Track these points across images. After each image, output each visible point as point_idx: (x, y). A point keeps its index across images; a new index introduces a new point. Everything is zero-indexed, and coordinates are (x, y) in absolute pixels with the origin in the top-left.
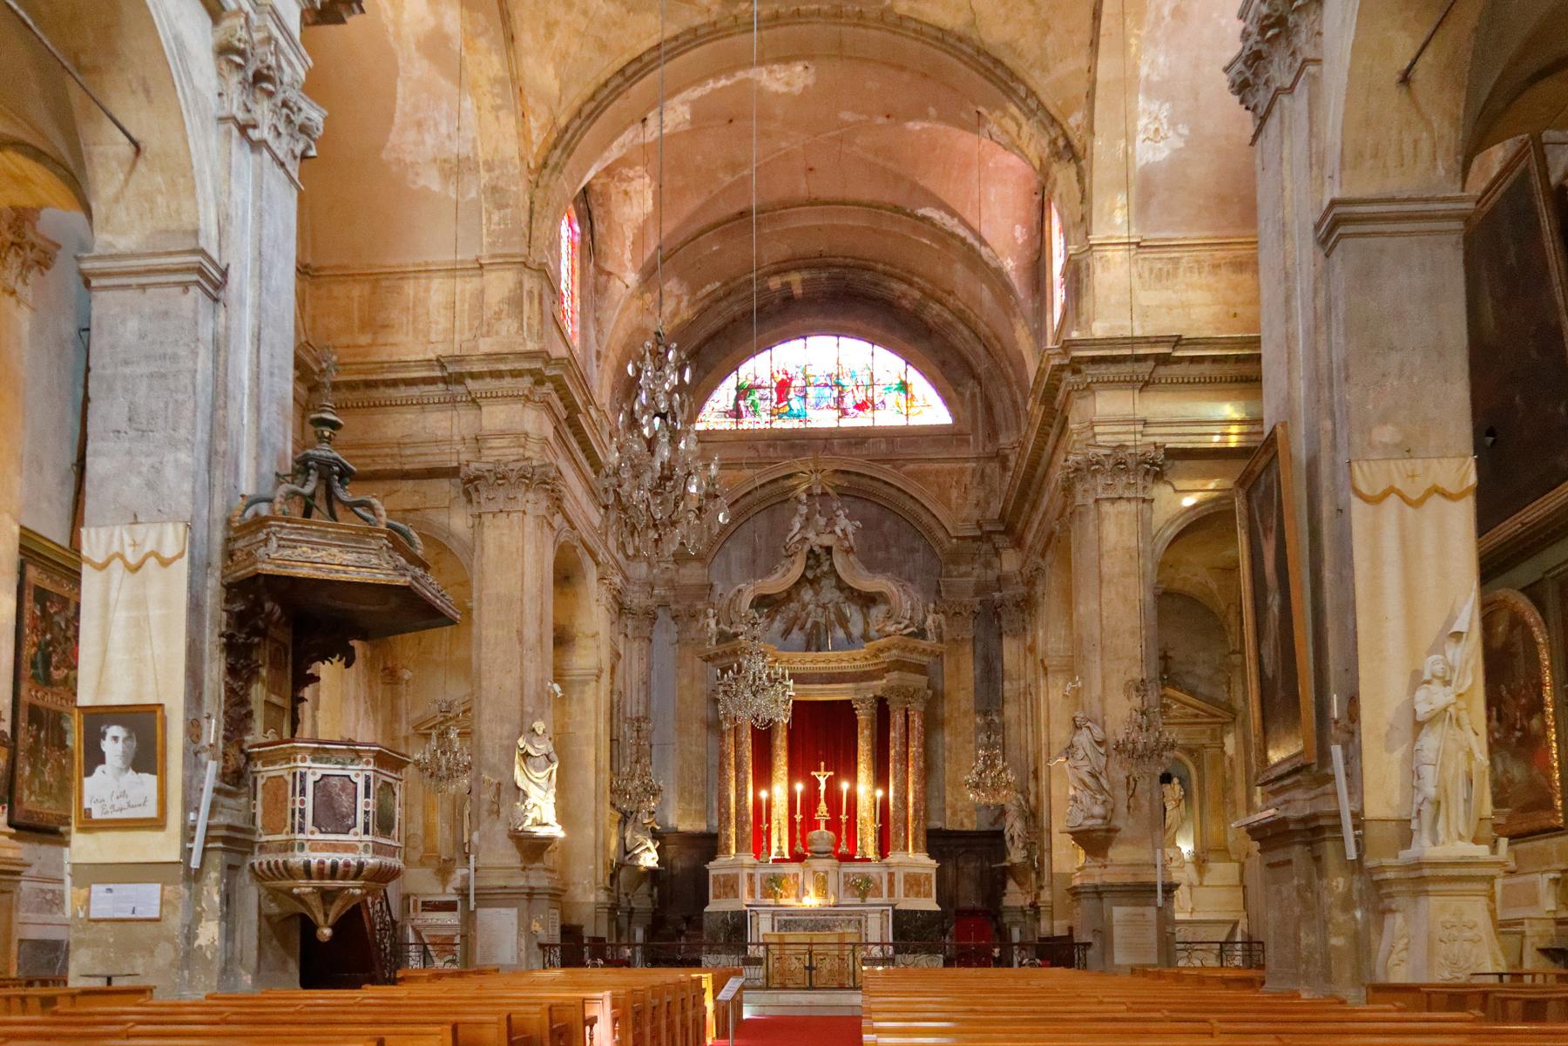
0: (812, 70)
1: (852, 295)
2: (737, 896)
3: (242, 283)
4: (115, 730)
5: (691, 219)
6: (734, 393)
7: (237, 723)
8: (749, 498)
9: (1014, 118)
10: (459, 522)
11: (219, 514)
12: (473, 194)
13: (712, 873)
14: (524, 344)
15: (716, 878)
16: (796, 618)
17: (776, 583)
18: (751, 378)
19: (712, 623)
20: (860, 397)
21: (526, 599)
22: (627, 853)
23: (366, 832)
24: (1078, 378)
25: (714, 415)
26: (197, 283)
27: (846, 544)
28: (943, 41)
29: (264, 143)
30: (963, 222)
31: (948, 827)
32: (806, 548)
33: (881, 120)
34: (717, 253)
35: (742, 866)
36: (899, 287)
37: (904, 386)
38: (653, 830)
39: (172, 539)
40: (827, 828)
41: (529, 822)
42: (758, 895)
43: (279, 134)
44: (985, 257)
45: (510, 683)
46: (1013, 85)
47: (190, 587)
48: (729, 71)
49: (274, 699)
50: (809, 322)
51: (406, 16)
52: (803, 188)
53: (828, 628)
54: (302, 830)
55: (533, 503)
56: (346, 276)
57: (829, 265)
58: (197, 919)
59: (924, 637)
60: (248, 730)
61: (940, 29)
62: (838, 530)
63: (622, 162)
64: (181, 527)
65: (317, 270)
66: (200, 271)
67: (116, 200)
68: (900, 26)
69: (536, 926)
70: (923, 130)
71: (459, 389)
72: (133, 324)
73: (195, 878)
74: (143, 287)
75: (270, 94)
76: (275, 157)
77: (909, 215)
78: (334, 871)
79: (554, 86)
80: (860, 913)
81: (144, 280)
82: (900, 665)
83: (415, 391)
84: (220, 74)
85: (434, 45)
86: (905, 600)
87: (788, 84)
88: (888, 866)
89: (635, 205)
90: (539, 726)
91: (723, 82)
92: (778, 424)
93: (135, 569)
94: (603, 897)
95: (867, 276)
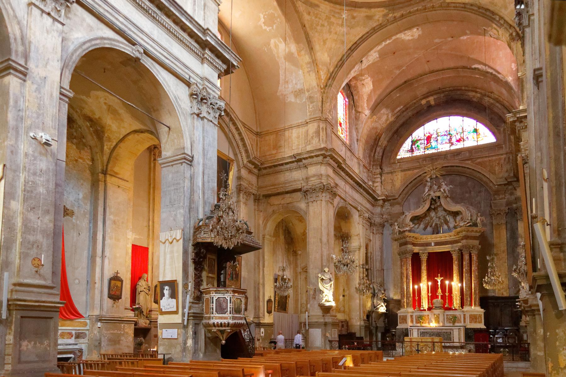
0: (420, 29)
1: (454, 101)
2: (406, 323)
3: (199, 158)
4: (167, 287)
5: (387, 87)
6: (411, 143)
7: (198, 283)
8: (416, 180)
9: (495, 29)
10: (302, 205)
11: (192, 226)
12: (304, 100)
13: (399, 315)
14: (320, 146)
15: (400, 316)
16: (428, 223)
17: (420, 211)
18: (417, 137)
19: (397, 227)
20: (458, 137)
21: (323, 229)
22: (375, 307)
23: (230, 313)
24: (522, 124)
25: (403, 153)
26: (184, 162)
27: (445, 194)
28: (465, 8)
29: (204, 117)
30: (489, 67)
31: (497, 295)
32: (430, 198)
33: (450, 39)
34: (399, 96)
35: (408, 312)
36: (471, 94)
37: (476, 131)
38: (384, 299)
39: (178, 234)
40: (441, 298)
41: (324, 301)
42: (414, 323)
43: (210, 113)
44: (501, 78)
45: (318, 256)
46: (494, 17)
47: (184, 247)
48: (389, 38)
49: (210, 275)
50: (439, 113)
51: (280, 51)
52: (427, 68)
53: (441, 225)
54: (212, 313)
55: (325, 196)
56: (268, 133)
57: (443, 92)
58: (187, 338)
59: (477, 226)
60: (202, 285)
61: (464, 4)
62: (442, 190)
63: (361, 74)
64: (181, 230)
65: (261, 133)
66: (185, 159)
67: (166, 143)
68: (449, 7)
69: (328, 335)
70: (467, 38)
71: (300, 163)
72: (170, 176)
73: (185, 327)
74: (172, 165)
75: (206, 103)
76: (208, 120)
77: (469, 69)
78: (221, 325)
79: (328, 59)
80: (451, 329)
81: (172, 163)
82: (466, 237)
83: (288, 166)
84: (191, 102)
85: (289, 57)
86: (467, 212)
87: (412, 36)
88: (463, 312)
89: (367, 88)
90: (326, 270)
91: (388, 42)
92: (427, 152)
93: (171, 243)
94: (362, 323)
95: (459, 92)
